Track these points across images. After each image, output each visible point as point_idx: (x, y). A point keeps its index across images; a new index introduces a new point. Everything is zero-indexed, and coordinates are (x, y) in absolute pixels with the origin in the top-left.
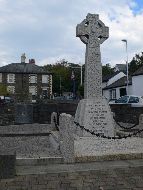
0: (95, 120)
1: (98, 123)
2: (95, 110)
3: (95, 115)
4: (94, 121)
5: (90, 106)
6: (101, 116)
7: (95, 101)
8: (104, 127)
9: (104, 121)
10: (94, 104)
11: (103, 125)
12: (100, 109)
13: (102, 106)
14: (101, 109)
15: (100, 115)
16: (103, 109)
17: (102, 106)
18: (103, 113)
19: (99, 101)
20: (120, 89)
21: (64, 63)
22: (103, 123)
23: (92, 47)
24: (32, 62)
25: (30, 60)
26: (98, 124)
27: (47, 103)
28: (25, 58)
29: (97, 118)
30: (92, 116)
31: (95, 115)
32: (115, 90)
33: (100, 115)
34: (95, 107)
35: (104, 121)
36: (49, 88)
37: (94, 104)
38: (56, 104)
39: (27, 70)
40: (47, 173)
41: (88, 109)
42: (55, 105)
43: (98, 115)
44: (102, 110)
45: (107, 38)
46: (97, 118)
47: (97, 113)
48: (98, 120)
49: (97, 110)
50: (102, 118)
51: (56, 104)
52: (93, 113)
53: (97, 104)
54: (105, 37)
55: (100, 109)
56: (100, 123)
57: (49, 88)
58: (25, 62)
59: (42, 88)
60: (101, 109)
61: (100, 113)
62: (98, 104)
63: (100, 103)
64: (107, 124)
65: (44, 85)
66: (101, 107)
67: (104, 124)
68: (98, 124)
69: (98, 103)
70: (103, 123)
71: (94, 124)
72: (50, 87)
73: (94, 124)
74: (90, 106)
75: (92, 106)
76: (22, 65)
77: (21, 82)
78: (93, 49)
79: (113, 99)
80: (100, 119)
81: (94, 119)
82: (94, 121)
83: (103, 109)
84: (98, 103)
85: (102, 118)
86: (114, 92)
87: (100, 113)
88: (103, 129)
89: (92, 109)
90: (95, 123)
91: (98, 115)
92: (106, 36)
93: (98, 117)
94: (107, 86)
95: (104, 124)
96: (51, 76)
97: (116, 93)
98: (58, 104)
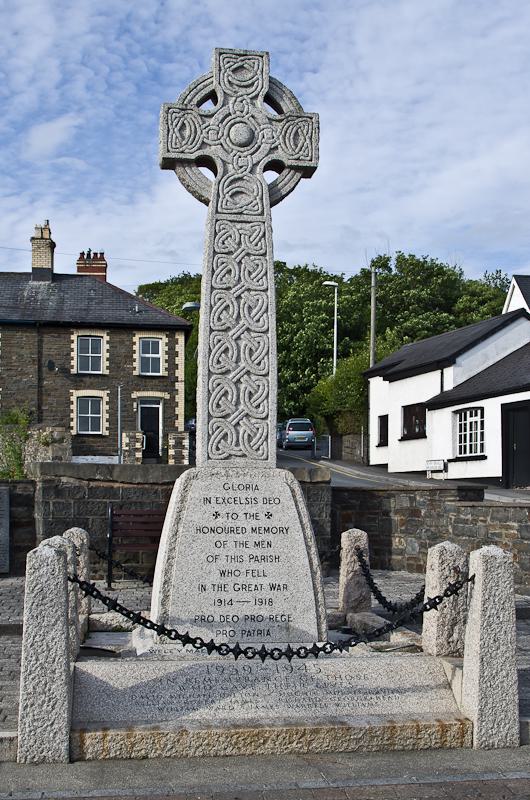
0: (233, 566)
1: (241, 580)
2: (230, 523)
3: (231, 544)
4: (223, 573)
5: (208, 500)
6: (258, 552)
7: (236, 481)
8: (271, 601)
9: (274, 573)
10: (231, 493)
11: (266, 594)
12: (255, 516)
13: (267, 501)
14: (262, 516)
15: (257, 544)
16: (269, 515)
17: (267, 501)
18: (269, 537)
19: (256, 481)
20: (506, 409)
21: (382, 262)
22: (266, 582)
23: (233, 217)
24: (92, 262)
25: (83, 254)
26: (244, 587)
27: (72, 480)
28: (52, 245)
29: (239, 559)
30: (217, 551)
31: (231, 544)
32: (482, 409)
33: (257, 544)
34: (239, 510)
35: (274, 573)
36: (167, 396)
37: (231, 493)
38: (116, 485)
39: (59, 310)
40: (421, 781)
41: (197, 515)
42: (111, 492)
43: (245, 544)
44: (264, 522)
45: (308, 172)
46: (239, 559)
47: (240, 537)
48: (243, 567)
49: (241, 522)
50: (264, 559)
51: (116, 485)
52: (223, 537)
53: (242, 495)
54: (297, 169)
55: (255, 516)
56: (254, 582)
57: (167, 396)
58: (51, 270)
59: (134, 396)
60: (262, 516)
61: (257, 538)
62: (251, 494)
63: (257, 488)
64: (285, 587)
65: (144, 381)
66: (261, 508)
67: (273, 587)
68: (244, 587)
69: (247, 488)
70: (266, 582)
71: (222, 588)
72: (173, 392)
73: (222, 588)
74: (208, 500)
75: (220, 500)
76: (35, 283)
77: (32, 369)
78: (239, 226)
79: (468, 454)
80: (254, 565)
81: (222, 563)
82: (223, 573)
83: (269, 515)
84: (247, 488)
85: (264, 559)
86: (474, 419)
87: (257, 538)
88: (265, 611)
89: (216, 515)
90: (229, 580)
91: (245, 544)
92: (301, 164)
93: (246, 552)
94: (446, 389)
95: (273, 587)
96: (181, 338)
97: (482, 422)
98: (126, 486)
